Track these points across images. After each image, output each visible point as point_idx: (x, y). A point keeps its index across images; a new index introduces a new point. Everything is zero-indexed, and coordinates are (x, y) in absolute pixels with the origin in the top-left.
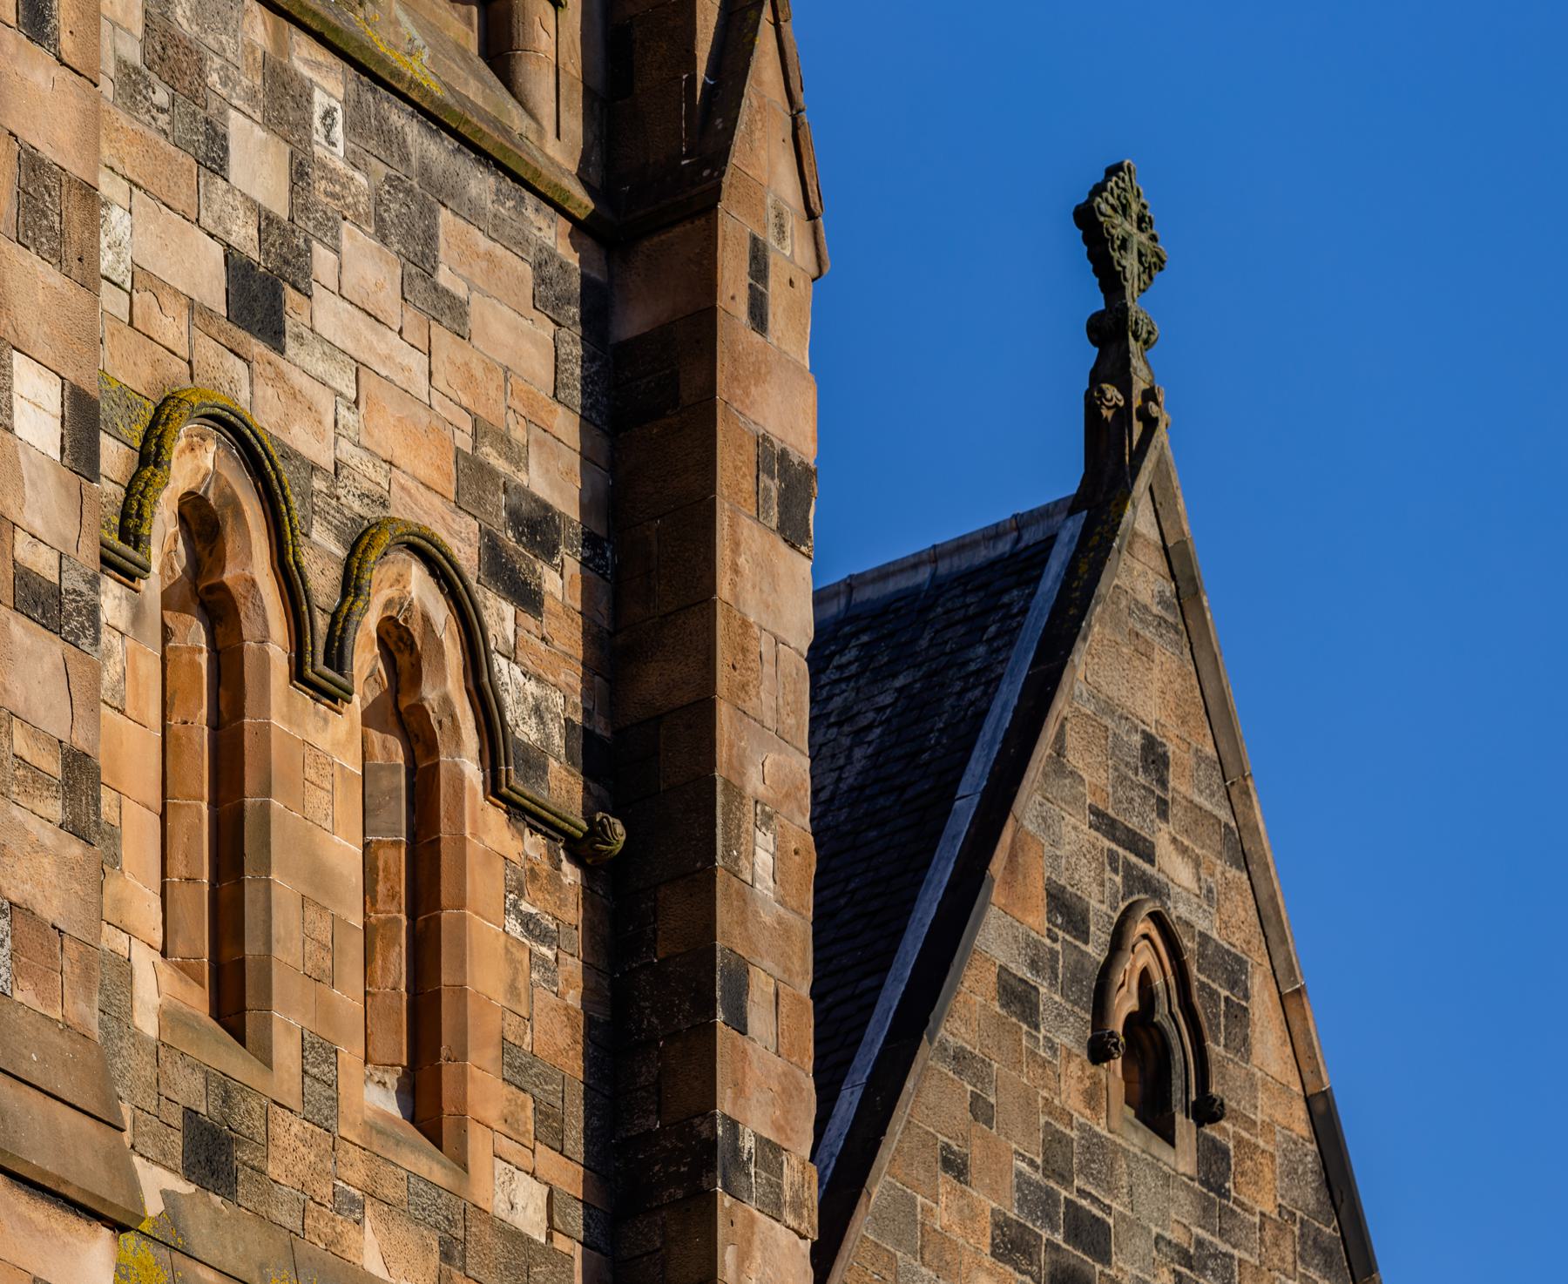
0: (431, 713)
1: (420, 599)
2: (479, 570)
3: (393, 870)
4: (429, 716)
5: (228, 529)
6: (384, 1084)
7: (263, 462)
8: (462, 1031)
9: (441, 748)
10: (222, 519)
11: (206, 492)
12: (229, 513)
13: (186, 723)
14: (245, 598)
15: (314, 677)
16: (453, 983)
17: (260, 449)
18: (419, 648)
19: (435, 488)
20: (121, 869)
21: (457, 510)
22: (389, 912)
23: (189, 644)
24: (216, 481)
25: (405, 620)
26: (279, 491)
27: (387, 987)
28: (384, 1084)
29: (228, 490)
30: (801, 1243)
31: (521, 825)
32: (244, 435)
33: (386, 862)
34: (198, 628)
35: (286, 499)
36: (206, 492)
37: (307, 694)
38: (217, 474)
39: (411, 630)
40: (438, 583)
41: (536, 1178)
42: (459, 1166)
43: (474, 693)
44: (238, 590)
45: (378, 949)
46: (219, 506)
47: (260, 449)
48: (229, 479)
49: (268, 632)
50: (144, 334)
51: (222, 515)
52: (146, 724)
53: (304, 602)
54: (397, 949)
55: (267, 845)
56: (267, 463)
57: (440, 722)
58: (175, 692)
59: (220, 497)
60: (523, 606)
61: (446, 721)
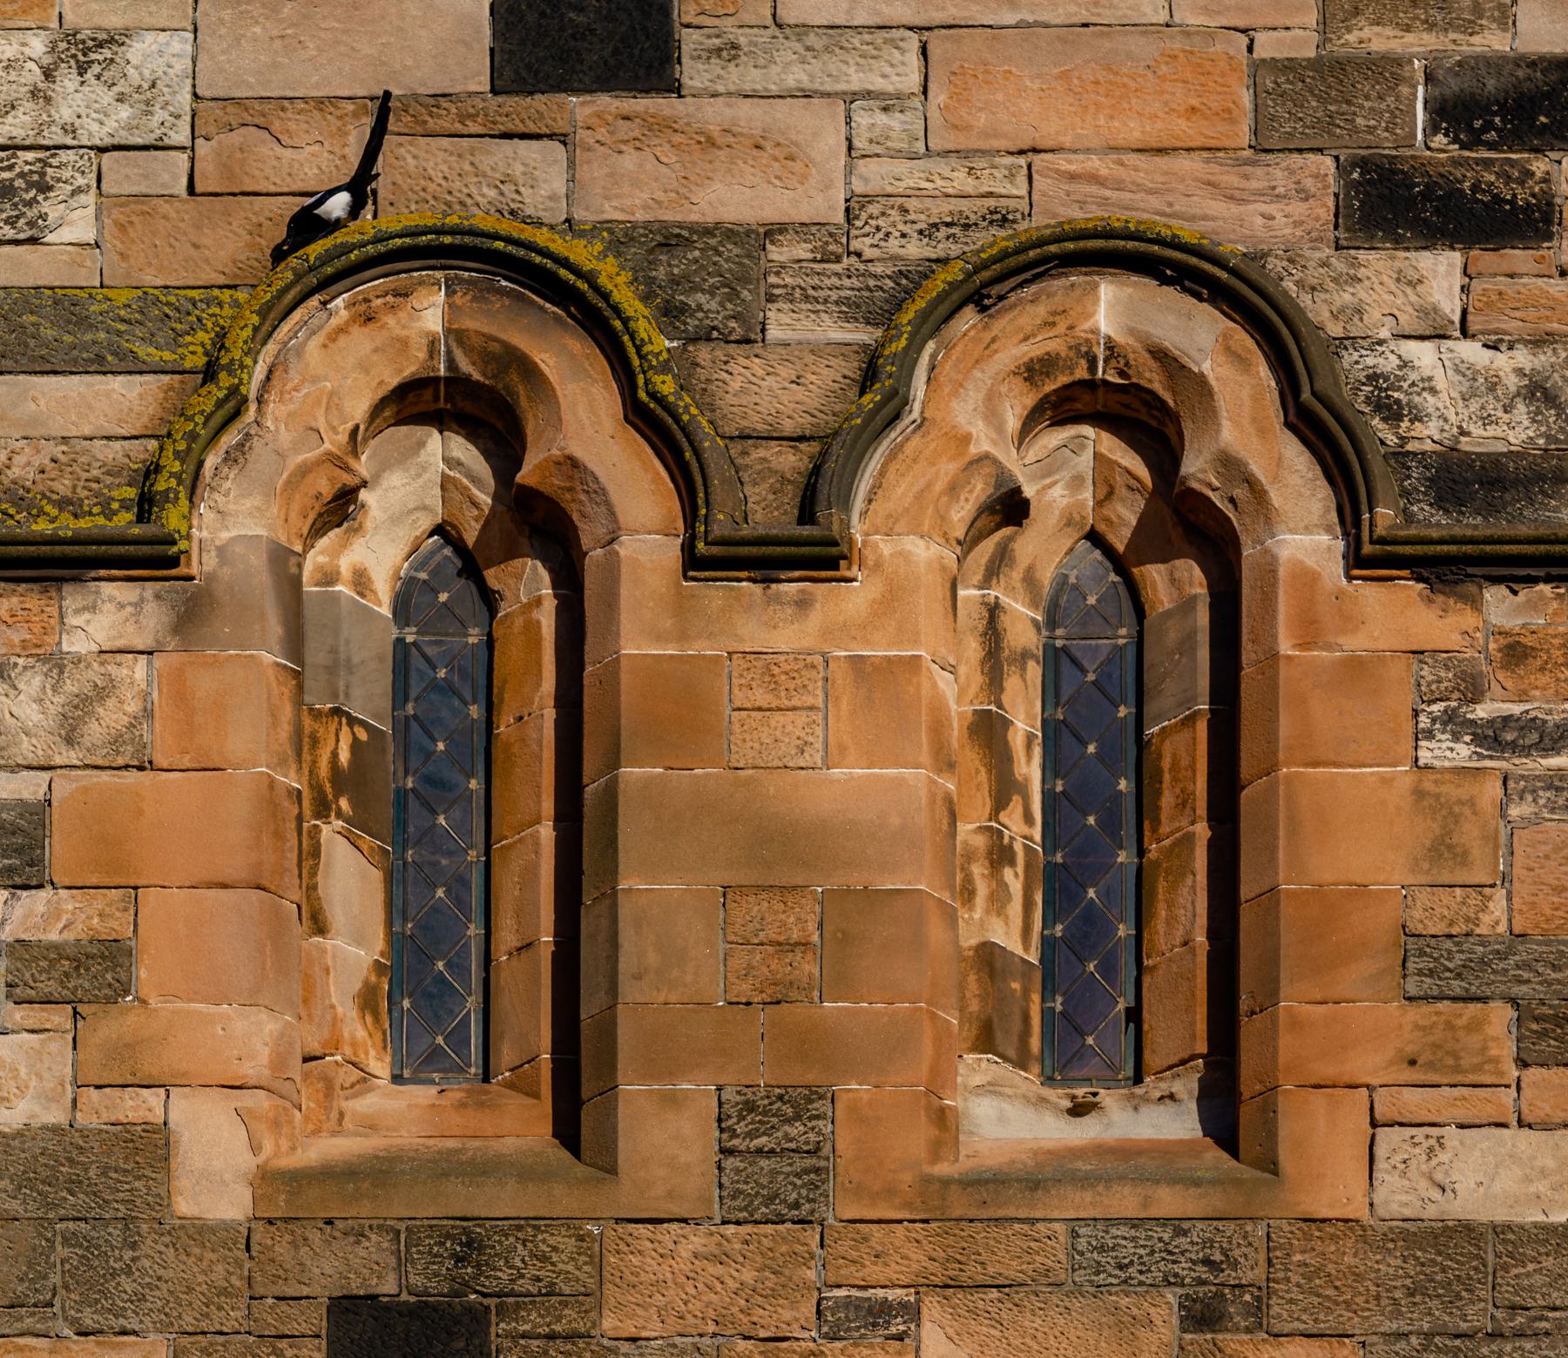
0: (1210, 494)
1: (1132, 331)
2: (1336, 227)
3: (1185, 763)
4: (1208, 499)
5: (523, 402)
6: (1172, 1097)
7: (555, 275)
8: (1271, 962)
9: (1243, 538)
10: (510, 393)
11: (451, 364)
12: (514, 377)
13: (521, 718)
14: (570, 489)
15: (715, 550)
16: (1258, 892)
17: (538, 259)
18: (1171, 403)
19: (1178, 144)
20: (137, 998)
21: (1263, 156)
22: (1178, 830)
23: (524, 600)
24: (460, 342)
25: (1122, 374)
26: (601, 304)
27: (1174, 946)
28: (1172, 1097)
29: (495, 347)
30: (248, 1156)
31: (1472, 588)
32: (496, 252)
33: (1174, 756)
34: (534, 568)
35: (617, 310)
36: (451, 364)
37: (739, 580)
38: (455, 334)
39: (1143, 383)
40: (1185, 290)
41: (1530, 1126)
42: (1264, 1170)
43: (1301, 426)
44: (553, 484)
45: (1160, 897)
46: (494, 377)
47: (538, 259)
48: (486, 330)
49: (616, 521)
50: (234, 195)
51: (506, 388)
52: (218, 765)
53: (686, 445)
54: (1189, 882)
55: (611, 842)
56: (563, 272)
57: (1232, 500)
58: (505, 681)
59: (486, 363)
60: (1487, 241)
61: (1240, 492)
